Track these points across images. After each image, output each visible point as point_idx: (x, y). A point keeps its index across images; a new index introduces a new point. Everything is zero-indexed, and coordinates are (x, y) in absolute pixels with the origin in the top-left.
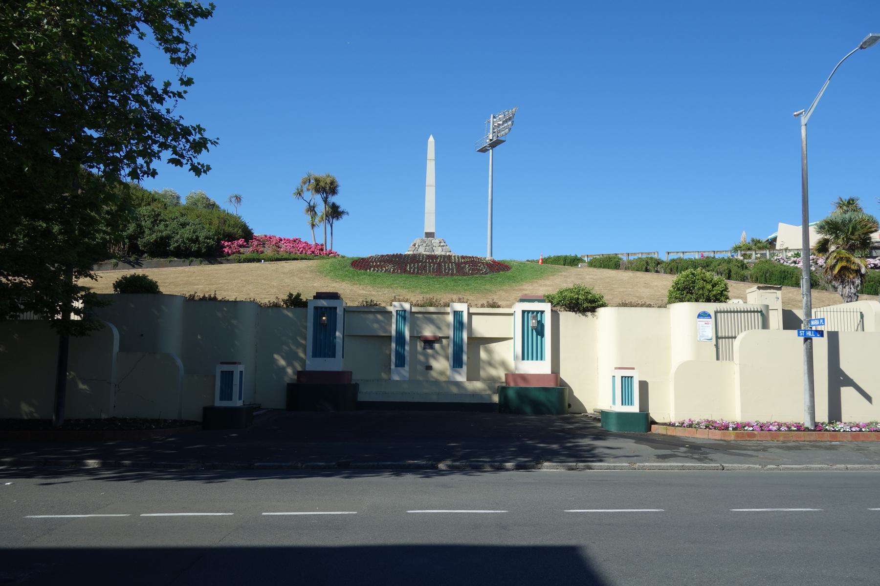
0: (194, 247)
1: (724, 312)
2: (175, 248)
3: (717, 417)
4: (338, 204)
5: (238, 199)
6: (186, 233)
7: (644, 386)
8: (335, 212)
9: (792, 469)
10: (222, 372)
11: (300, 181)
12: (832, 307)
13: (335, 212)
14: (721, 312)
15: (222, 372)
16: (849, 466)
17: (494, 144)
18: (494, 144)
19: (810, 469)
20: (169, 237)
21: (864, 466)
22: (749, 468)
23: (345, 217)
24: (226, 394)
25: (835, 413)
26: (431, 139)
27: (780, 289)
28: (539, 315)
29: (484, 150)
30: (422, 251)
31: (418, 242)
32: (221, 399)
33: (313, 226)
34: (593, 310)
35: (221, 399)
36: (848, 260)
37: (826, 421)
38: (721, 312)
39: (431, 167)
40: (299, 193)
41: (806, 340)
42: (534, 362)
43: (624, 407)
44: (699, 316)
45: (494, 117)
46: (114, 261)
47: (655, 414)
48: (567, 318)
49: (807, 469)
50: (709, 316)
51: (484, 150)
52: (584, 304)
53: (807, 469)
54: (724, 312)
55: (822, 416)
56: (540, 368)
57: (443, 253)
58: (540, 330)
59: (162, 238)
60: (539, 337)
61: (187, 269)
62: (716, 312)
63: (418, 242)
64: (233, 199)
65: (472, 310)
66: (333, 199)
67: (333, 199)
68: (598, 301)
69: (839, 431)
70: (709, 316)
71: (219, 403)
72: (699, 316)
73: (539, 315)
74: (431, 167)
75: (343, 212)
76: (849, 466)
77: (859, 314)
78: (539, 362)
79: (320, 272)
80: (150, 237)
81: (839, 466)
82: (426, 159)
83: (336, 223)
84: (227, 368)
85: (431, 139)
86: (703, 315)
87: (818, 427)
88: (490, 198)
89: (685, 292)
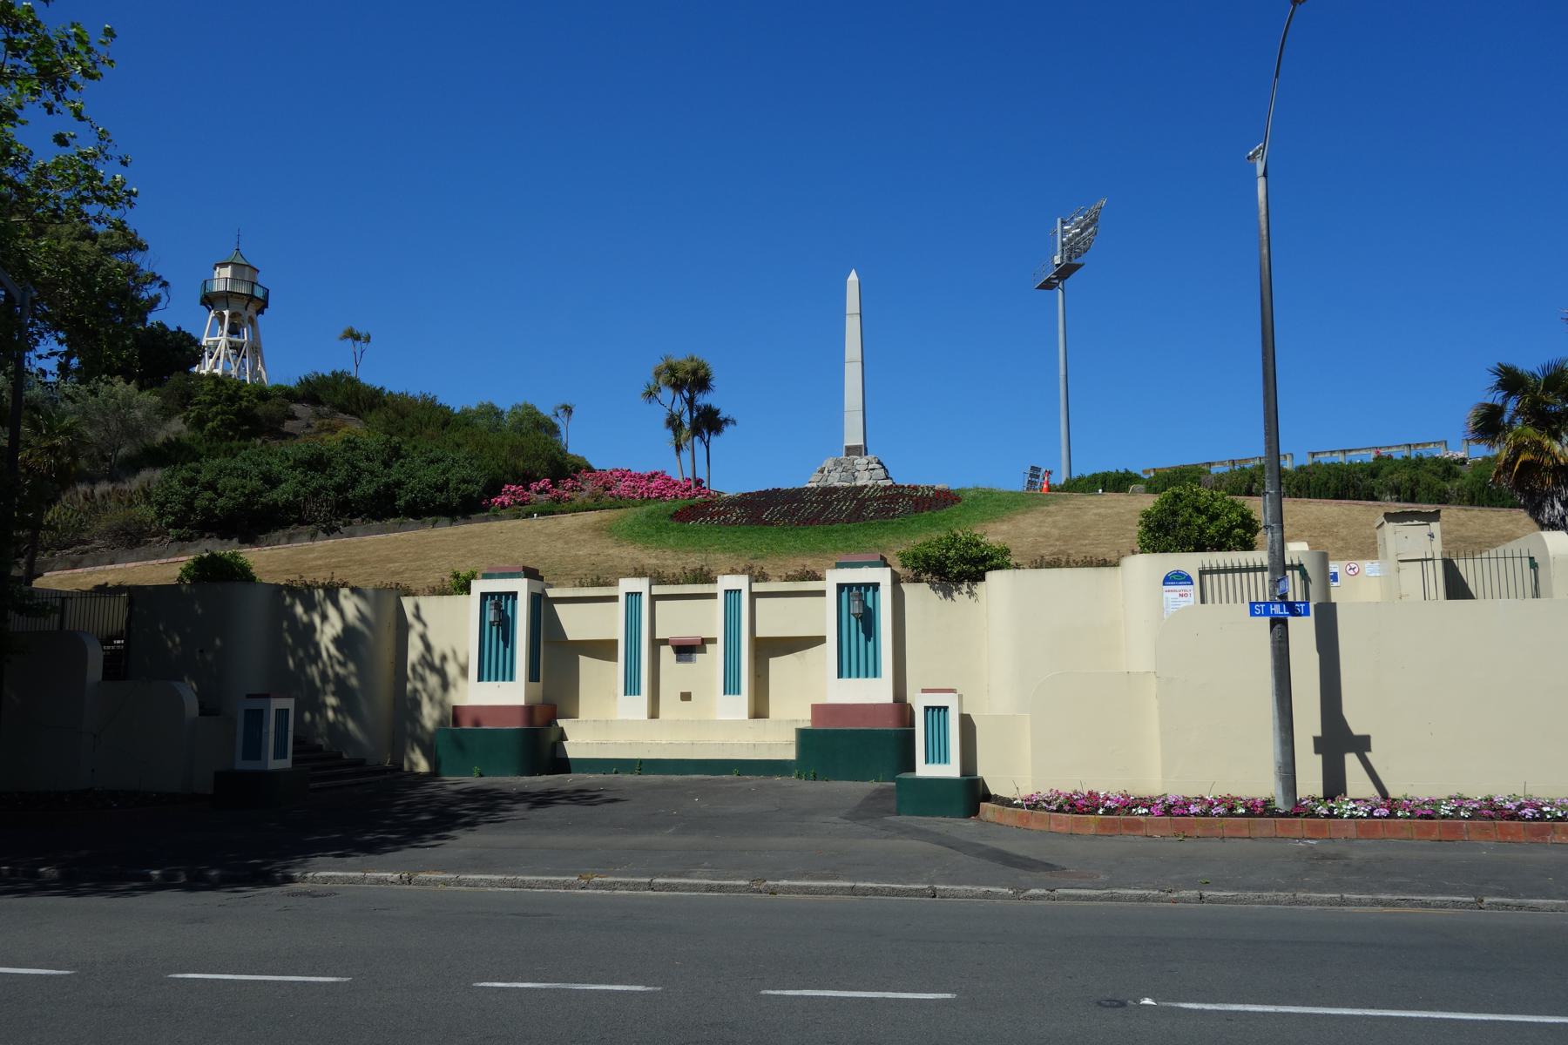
0: (441, 498)
1: (1218, 571)
2: (407, 502)
3: (1108, 784)
4: (716, 406)
5: (568, 410)
6: (432, 475)
7: (967, 724)
8: (709, 423)
9: (1079, 898)
10: (247, 711)
11: (651, 373)
12: (1500, 550)
13: (709, 423)
14: (1211, 572)
15: (247, 711)
16: (1301, 895)
17: (1065, 272)
18: (1065, 272)
19: (1119, 898)
20: (399, 484)
21: (1241, 895)
22: (986, 895)
23: (728, 430)
24: (254, 748)
25: (1334, 784)
26: (853, 277)
27: (1435, 516)
28: (870, 594)
29: (1048, 285)
30: (835, 480)
31: (828, 463)
32: (245, 757)
33: (678, 448)
34: (979, 577)
35: (245, 757)
36: (1539, 448)
37: (1319, 793)
38: (1211, 572)
39: (853, 327)
40: (650, 395)
41: (1274, 622)
42: (862, 680)
43: (930, 766)
44: (1168, 580)
45: (1064, 223)
46: (311, 528)
47: (998, 776)
48: (919, 596)
49: (1112, 899)
50: (1188, 580)
51: (1048, 285)
52: (959, 569)
53: (1112, 899)
54: (1218, 571)
55: (1310, 782)
56: (876, 691)
57: (870, 483)
58: (868, 621)
59: (387, 485)
60: (862, 636)
61: (422, 532)
62: (1202, 573)
63: (828, 463)
64: (560, 412)
65: (757, 587)
66: (703, 400)
67: (703, 400)
68: (992, 558)
69: (1340, 816)
70: (1188, 580)
71: (241, 765)
72: (1168, 580)
73: (870, 594)
74: (853, 327)
75: (726, 421)
76: (1206, 894)
77: (1526, 562)
78: (871, 680)
79: (598, 530)
80: (366, 488)
81: (1184, 893)
82: (845, 315)
83: (715, 440)
84: (255, 704)
85: (853, 277)
86: (1175, 578)
87: (1298, 811)
88: (1062, 372)
89: (1161, 534)
